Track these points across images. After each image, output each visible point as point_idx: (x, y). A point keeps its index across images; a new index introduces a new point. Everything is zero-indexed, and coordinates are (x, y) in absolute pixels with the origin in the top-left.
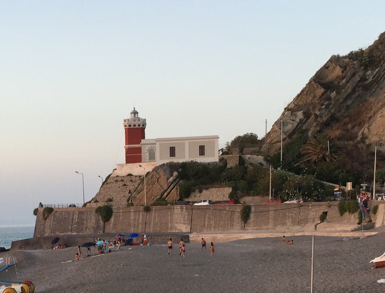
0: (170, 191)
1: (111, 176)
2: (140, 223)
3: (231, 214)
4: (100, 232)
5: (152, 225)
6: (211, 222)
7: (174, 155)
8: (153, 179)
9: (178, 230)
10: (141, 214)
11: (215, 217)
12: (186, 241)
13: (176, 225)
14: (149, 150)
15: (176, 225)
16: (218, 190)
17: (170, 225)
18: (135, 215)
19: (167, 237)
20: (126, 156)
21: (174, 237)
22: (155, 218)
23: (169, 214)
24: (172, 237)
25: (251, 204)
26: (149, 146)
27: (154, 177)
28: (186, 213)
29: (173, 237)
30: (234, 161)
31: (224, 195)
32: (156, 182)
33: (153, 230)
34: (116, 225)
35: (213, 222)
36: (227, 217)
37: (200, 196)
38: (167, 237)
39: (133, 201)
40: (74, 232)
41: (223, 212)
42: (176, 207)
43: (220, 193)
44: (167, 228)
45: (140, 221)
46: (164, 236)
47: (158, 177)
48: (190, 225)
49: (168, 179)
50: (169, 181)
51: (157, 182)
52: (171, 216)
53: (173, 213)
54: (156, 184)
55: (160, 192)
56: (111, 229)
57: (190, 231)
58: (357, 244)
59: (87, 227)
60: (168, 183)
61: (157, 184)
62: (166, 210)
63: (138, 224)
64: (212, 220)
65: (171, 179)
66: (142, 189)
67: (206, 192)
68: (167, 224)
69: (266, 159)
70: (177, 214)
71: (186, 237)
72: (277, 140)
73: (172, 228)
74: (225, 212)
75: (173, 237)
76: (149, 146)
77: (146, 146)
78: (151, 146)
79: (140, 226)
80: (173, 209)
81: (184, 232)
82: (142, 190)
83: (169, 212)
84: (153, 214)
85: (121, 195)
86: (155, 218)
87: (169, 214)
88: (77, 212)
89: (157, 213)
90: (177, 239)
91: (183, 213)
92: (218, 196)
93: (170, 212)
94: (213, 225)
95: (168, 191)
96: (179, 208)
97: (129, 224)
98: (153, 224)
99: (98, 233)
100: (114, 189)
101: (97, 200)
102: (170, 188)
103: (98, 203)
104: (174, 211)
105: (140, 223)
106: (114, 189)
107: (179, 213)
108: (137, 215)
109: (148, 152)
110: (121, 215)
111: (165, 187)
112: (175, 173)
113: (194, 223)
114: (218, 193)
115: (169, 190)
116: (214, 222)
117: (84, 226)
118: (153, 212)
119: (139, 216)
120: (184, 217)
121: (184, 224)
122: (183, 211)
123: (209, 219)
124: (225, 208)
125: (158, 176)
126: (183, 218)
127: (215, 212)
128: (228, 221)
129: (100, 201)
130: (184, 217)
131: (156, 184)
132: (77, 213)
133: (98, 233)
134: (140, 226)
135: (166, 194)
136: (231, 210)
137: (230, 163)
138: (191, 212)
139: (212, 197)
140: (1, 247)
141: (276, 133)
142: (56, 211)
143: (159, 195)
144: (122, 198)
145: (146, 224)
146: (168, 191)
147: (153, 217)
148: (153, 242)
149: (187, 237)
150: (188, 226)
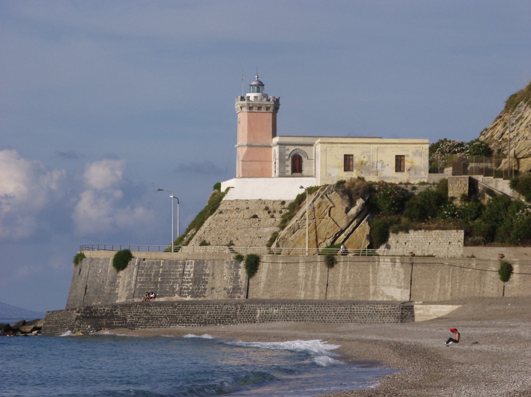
0: (351, 231)
1: (224, 199)
2: (317, 283)
3: (481, 273)
4: (239, 297)
5: (340, 287)
6: (446, 286)
7: (402, 169)
8: (321, 208)
9: (387, 297)
10: (318, 269)
11: (452, 277)
12: (409, 314)
13: (383, 288)
14: (292, 155)
15: (383, 288)
16: (440, 234)
17: (372, 289)
18: (308, 269)
19: (374, 307)
20: (440, 173)
21: (387, 307)
22: (344, 276)
23: (371, 270)
24: (384, 307)
25: (514, 260)
26: (292, 148)
27: (323, 206)
28: (401, 270)
29: (387, 308)
30: (460, 186)
31: (450, 243)
32: (326, 214)
33: (340, 296)
34: (269, 285)
35: (448, 285)
36: (473, 278)
37: (406, 241)
38: (374, 307)
39: (281, 246)
40: (186, 297)
41: (466, 270)
42: (383, 259)
43: (443, 239)
44: (368, 293)
45: (318, 279)
46: (370, 306)
47: (330, 206)
48: (409, 290)
49: (347, 210)
50: (350, 213)
51: (328, 215)
52: (375, 273)
53: (378, 269)
54: (327, 219)
55: (333, 234)
56: (261, 292)
57: (410, 300)
58: (494, 368)
59: (213, 289)
60: (348, 218)
61: (329, 218)
62: (365, 263)
63: (313, 285)
64: (448, 282)
65: (353, 211)
66: (299, 226)
67: (418, 236)
68: (367, 286)
69: (514, 185)
70: (385, 270)
71: (408, 308)
72: (527, 153)
73: (375, 293)
74: (470, 270)
75: (385, 308)
76: (292, 148)
77: (287, 147)
78: (294, 149)
79: (317, 289)
80: (377, 262)
81: (398, 300)
82: (300, 227)
83: (371, 266)
84: (341, 270)
85: (252, 233)
86: (344, 276)
87: (371, 270)
88: (194, 261)
89: (348, 268)
90: (393, 312)
91: (396, 269)
92: (440, 243)
93: (372, 267)
94: (450, 290)
95: (347, 231)
96: (389, 260)
97: (296, 285)
98: (342, 286)
99: (237, 299)
100: (236, 223)
101: (205, 241)
102: (351, 226)
103: (208, 247)
104: (378, 264)
105: (317, 283)
106: (236, 223)
107: (389, 270)
108: (312, 271)
109: (290, 158)
110: (280, 268)
111: (343, 224)
112: (360, 202)
113: (416, 286)
114: (440, 239)
115: (350, 228)
116: (450, 286)
117: (207, 286)
118: (342, 266)
119: (315, 271)
120: (398, 276)
121: (398, 287)
122: (396, 266)
123: (443, 279)
124: (470, 264)
125: (331, 205)
126: (396, 277)
127: (453, 270)
128: (474, 285)
129: (212, 243)
130: (398, 276)
131: (327, 219)
132: (194, 263)
133: (237, 299)
134: (317, 289)
135: (343, 236)
136: (480, 267)
137: (454, 189)
138: (410, 269)
139: (429, 244)
140: (1, 324)
141: (527, 141)
142: (144, 258)
143: (330, 238)
144: (256, 238)
145: (327, 285)
146: (347, 231)
147: (341, 275)
148: (349, 315)
149: (410, 307)
150: (406, 291)
